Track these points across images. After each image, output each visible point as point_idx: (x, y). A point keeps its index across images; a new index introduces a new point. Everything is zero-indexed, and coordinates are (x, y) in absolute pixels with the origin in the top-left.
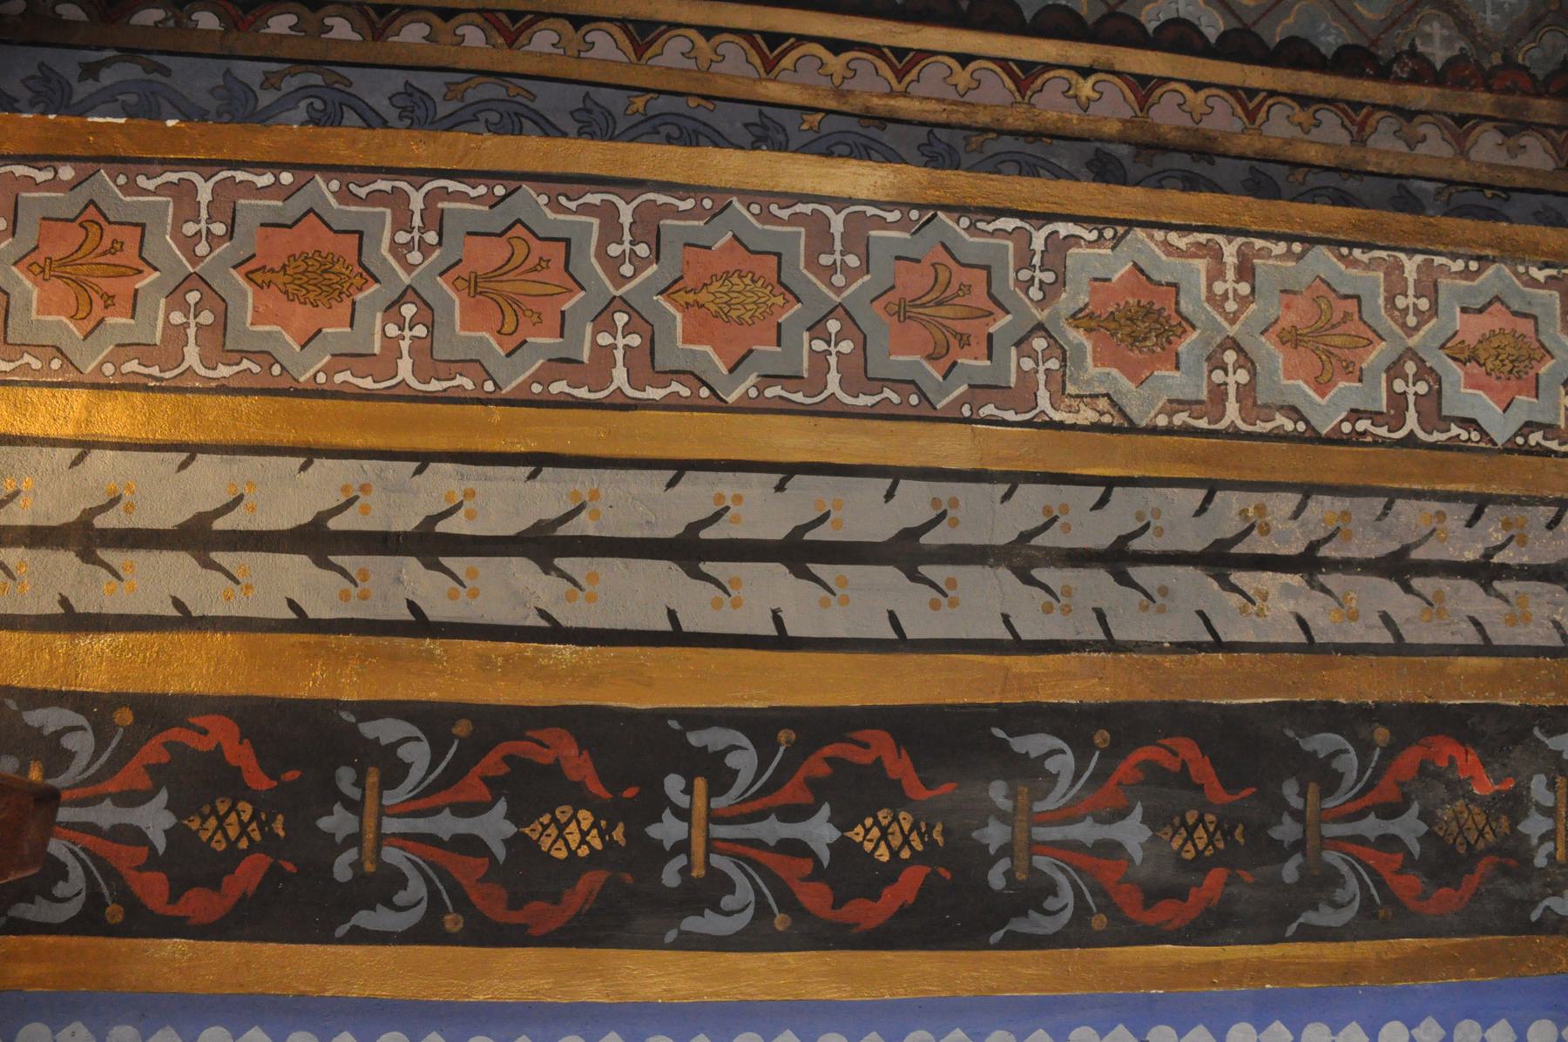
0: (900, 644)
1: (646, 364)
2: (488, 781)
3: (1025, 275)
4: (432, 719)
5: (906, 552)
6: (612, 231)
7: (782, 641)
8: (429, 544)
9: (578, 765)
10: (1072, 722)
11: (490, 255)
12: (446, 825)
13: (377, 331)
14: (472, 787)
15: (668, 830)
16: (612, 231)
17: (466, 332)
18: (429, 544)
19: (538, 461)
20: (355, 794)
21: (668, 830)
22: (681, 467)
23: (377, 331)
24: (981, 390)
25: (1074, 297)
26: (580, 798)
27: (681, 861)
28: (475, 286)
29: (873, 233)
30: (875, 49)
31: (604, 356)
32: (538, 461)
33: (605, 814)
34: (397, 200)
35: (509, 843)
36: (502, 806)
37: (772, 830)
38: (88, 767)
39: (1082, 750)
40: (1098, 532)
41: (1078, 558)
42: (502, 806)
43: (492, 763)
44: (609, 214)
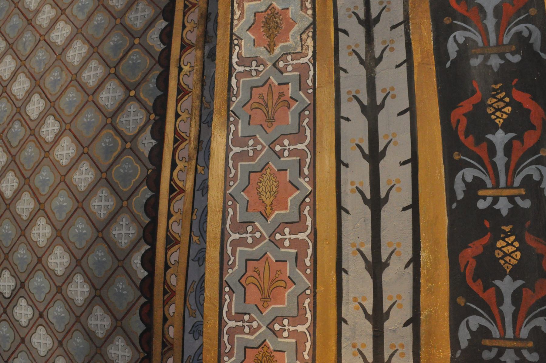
0: (412, 110)
1: (296, 225)
2: (485, 289)
3: (254, 73)
4: (457, 315)
5: (371, 111)
6: (242, 242)
7: (414, 161)
8: (378, 317)
9: (475, 248)
10: (441, 35)
11: (253, 293)
12: (508, 308)
13: (286, 341)
14: (489, 296)
15: (503, 206)
16: (242, 242)
17: (285, 303)
18: (378, 317)
19: (340, 270)
20: (489, 200)
21: (503, 206)
22: (340, 208)
23: (286, 341)
24: (301, 86)
25: (262, 52)
26: (491, 247)
27: (518, 200)
28: (266, 299)
29: (240, 135)
30: (175, 150)
31: (294, 243)
32: (340, 270)
33: (498, 235)
34: (232, 332)
35: (514, 279)
36: (497, 282)
37: (500, 159)
38: (475, 34)
39: (452, 28)
40: (358, 33)
41: (369, 39)
42: (497, 282)
43: (477, 287)
44: (236, 244)
